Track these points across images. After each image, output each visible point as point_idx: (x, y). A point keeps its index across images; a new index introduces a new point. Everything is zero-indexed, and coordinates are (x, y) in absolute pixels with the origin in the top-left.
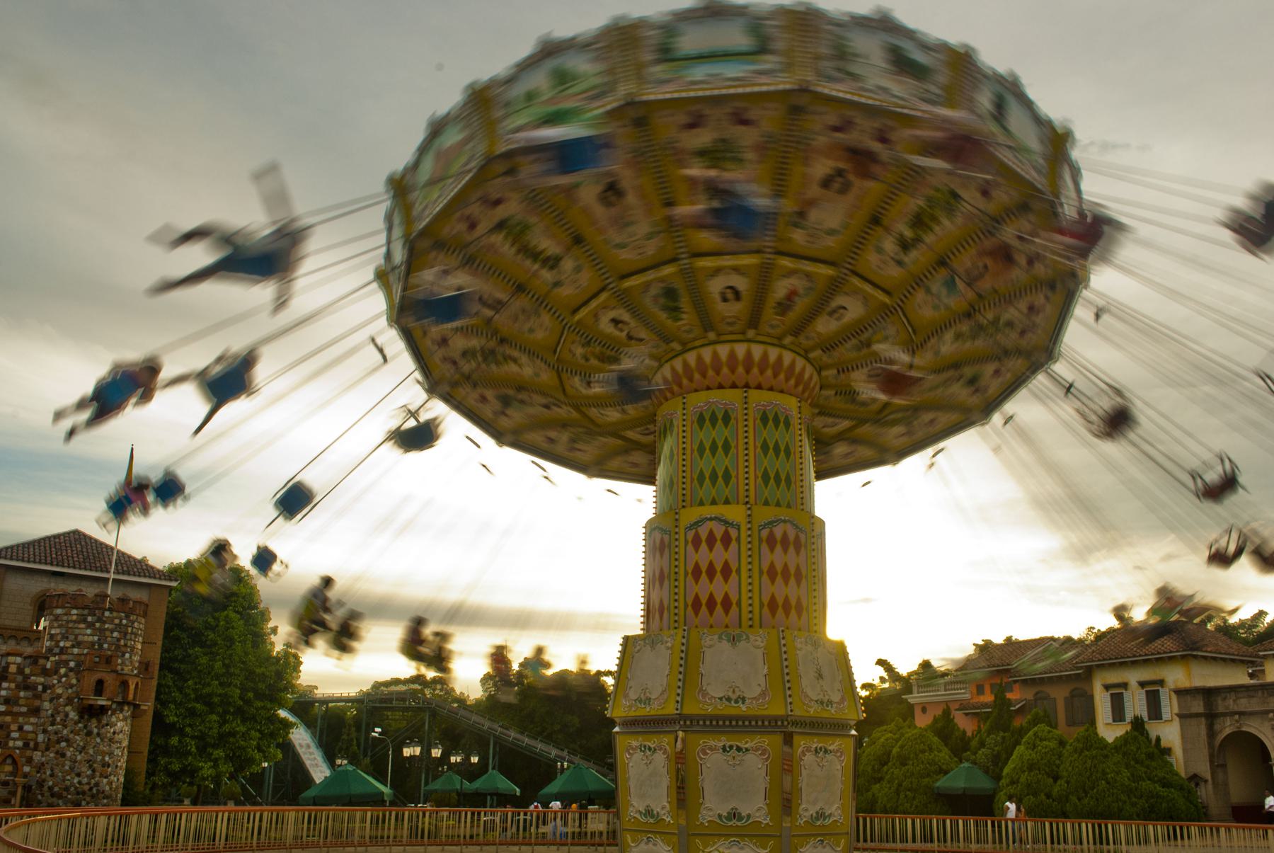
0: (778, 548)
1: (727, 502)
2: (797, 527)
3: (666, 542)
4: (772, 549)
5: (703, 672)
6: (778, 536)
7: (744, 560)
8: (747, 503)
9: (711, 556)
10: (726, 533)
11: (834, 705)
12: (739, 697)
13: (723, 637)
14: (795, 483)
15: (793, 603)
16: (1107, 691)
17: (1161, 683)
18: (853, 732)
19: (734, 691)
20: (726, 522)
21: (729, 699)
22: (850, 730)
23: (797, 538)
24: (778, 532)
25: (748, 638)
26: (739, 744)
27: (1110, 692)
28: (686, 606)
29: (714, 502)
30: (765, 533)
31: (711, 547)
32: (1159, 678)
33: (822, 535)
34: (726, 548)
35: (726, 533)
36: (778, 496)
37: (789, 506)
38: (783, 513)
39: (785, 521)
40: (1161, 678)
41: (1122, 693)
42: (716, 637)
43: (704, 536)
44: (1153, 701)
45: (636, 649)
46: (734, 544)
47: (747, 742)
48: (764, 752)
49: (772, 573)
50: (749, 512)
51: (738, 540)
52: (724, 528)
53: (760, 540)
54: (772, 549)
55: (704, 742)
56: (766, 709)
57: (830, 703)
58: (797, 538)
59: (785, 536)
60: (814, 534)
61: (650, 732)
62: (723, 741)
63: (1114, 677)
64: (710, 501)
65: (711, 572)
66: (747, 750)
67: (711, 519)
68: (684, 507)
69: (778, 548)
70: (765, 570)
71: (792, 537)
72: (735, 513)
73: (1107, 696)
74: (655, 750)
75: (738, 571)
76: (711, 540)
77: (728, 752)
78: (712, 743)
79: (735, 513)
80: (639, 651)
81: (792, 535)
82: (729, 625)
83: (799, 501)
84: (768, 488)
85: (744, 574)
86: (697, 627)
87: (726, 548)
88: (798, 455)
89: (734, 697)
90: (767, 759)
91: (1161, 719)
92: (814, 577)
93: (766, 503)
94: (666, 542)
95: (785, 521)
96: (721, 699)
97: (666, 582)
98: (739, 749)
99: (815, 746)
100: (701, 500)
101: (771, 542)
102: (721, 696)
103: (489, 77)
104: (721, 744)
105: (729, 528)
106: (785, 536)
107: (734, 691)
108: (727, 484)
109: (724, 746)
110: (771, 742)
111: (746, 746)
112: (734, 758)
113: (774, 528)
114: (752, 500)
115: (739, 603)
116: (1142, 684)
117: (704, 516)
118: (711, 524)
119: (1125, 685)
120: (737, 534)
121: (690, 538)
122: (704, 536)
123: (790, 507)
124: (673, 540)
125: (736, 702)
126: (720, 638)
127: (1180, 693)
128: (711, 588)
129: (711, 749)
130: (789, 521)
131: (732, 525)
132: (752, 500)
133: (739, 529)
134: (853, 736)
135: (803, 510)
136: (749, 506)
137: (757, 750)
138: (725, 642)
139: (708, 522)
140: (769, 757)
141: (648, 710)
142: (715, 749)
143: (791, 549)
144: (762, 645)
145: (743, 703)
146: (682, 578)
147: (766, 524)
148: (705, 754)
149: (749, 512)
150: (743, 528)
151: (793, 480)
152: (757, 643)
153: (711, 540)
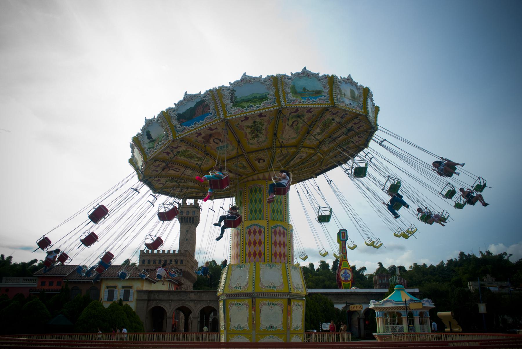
0: (278, 235)
1: (260, 219)
2: (284, 228)
3: (239, 232)
4: (275, 235)
5: (261, 278)
6: (278, 231)
7: (266, 240)
8: (267, 219)
9: (255, 237)
10: (260, 229)
11: (301, 289)
12: (273, 286)
13: (267, 265)
14: (283, 213)
15: (282, 254)
16: (107, 289)
17: (131, 287)
18: (304, 298)
19: (272, 284)
20: (260, 226)
21: (270, 287)
22: (303, 298)
23: (284, 232)
24: (278, 230)
25: (276, 266)
26: (273, 302)
27: (124, 289)
28: (246, 255)
29: (256, 219)
30: (273, 230)
31: (255, 234)
32: (131, 286)
33: (292, 231)
34: (260, 235)
35: (260, 229)
36: (256, 217)
37: (281, 221)
38: (279, 223)
39: (280, 226)
40: (132, 286)
41: (114, 290)
42: (265, 265)
43: (252, 231)
44: (127, 294)
45: (233, 269)
46: (263, 233)
47: (276, 302)
48: (282, 305)
49: (275, 243)
50: (268, 223)
51: (264, 232)
52: (259, 228)
53: (272, 232)
54: (275, 235)
55: (262, 302)
56: (247, 290)
57: (300, 289)
58: (284, 232)
59: (280, 231)
60: (289, 230)
61: (239, 298)
62: (268, 301)
63: (111, 283)
64: (254, 219)
65: (255, 243)
66: (276, 304)
67: (255, 225)
68: (245, 220)
69: (278, 235)
70: (273, 243)
71: (282, 232)
72: (263, 223)
73: (107, 291)
74: (242, 304)
75: (264, 243)
76: (255, 232)
77: (270, 305)
78: (233, 303)
79: (263, 223)
80: (234, 270)
81: (282, 230)
82: (261, 261)
83: (285, 219)
84: (256, 214)
85: (266, 244)
86: (260, 262)
87: (260, 235)
88: (284, 204)
89: (272, 286)
90: (283, 307)
91: (129, 300)
92: (289, 245)
93: (274, 220)
94: (239, 232)
95: (280, 226)
96: (267, 287)
97: (239, 246)
98: (273, 304)
99: (296, 303)
100: (260, 218)
101: (275, 233)
102: (267, 286)
103: (295, 73)
104: (267, 302)
105: (261, 228)
106: (280, 231)
107: (272, 284)
108: (260, 213)
109: (268, 303)
110: (248, 301)
111: (276, 303)
112: (272, 307)
113: (276, 228)
114: (269, 219)
115: (264, 254)
116: (123, 287)
117: (252, 224)
118: (255, 227)
119: (115, 287)
120: (264, 230)
121: (247, 232)
122: (252, 231)
123: (274, 220)
124: (241, 232)
125: (273, 288)
126: (266, 266)
127: (139, 292)
128: (255, 248)
129: (264, 304)
130: (281, 226)
131: (262, 227)
132: (269, 219)
133: (264, 229)
134: (305, 300)
135: (286, 222)
136: (268, 220)
137: (279, 304)
138: (268, 267)
139: (254, 226)
140: (248, 307)
141: (240, 291)
142: (233, 305)
143: (282, 236)
144: (280, 268)
145: (275, 288)
146: (245, 246)
147: (273, 227)
148: (262, 306)
149: (268, 223)
150: (266, 228)
151: (282, 212)
152: (279, 268)
153: (255, 232)
